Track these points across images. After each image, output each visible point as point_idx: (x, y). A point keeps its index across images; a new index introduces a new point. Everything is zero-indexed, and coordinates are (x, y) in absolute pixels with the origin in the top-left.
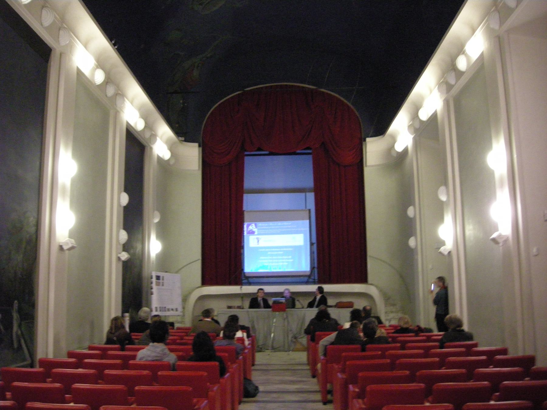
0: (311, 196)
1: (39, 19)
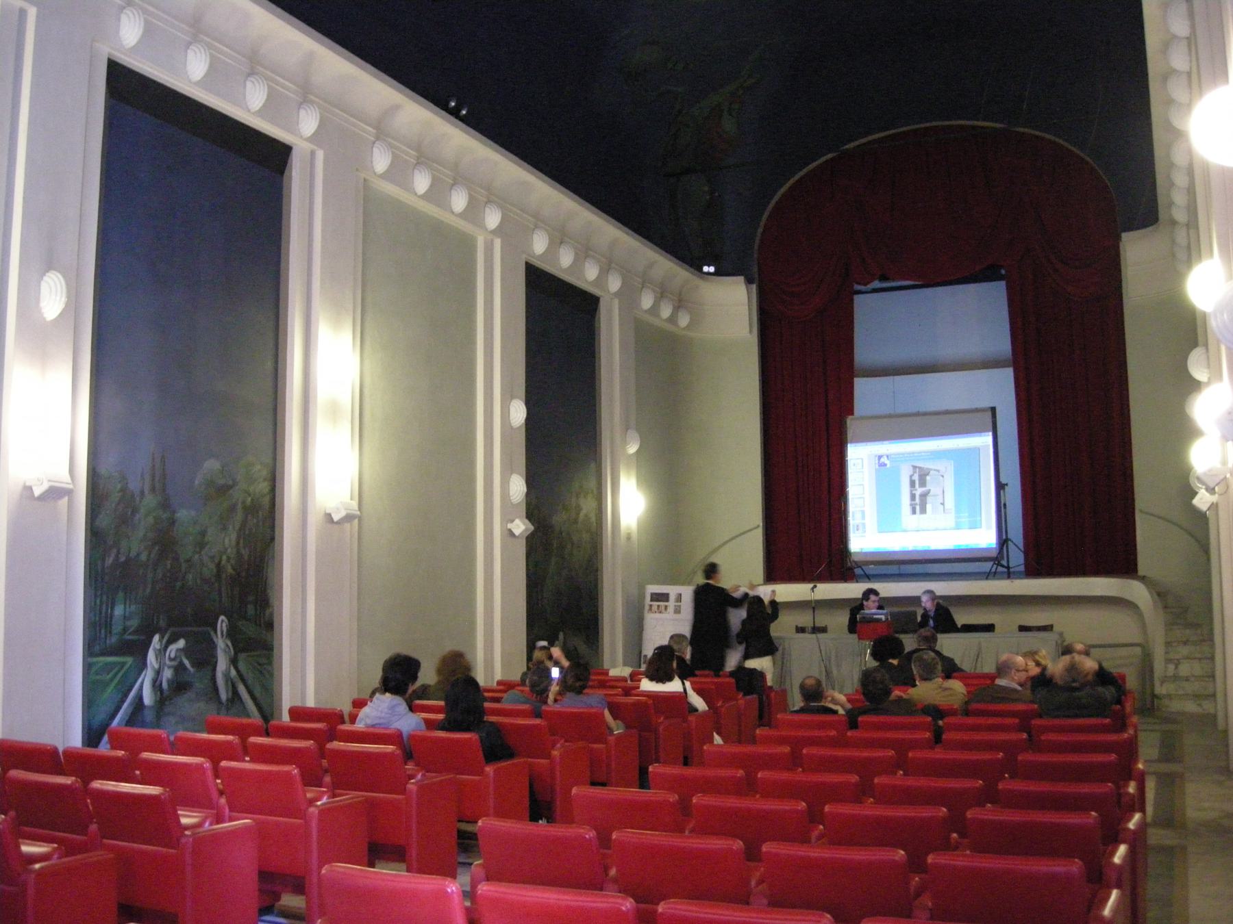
0: (1009, 372)
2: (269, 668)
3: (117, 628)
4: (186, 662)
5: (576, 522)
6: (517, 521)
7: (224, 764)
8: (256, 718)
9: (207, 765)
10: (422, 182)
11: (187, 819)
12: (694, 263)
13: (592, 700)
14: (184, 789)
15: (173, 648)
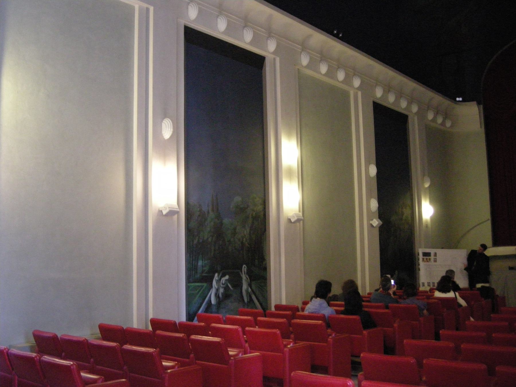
1: (242, 39)
3: (200, 270)
4: (230, 286)
5: (402, 219)
6: (375, 220)
7: (247, 328)
8: (260, 309)
9: (240, 329)
10: (324, 69)
11: (232, 352)
12: (453, 98)
13: (411, 302)
14: (230, 338)
15: (224, 280)
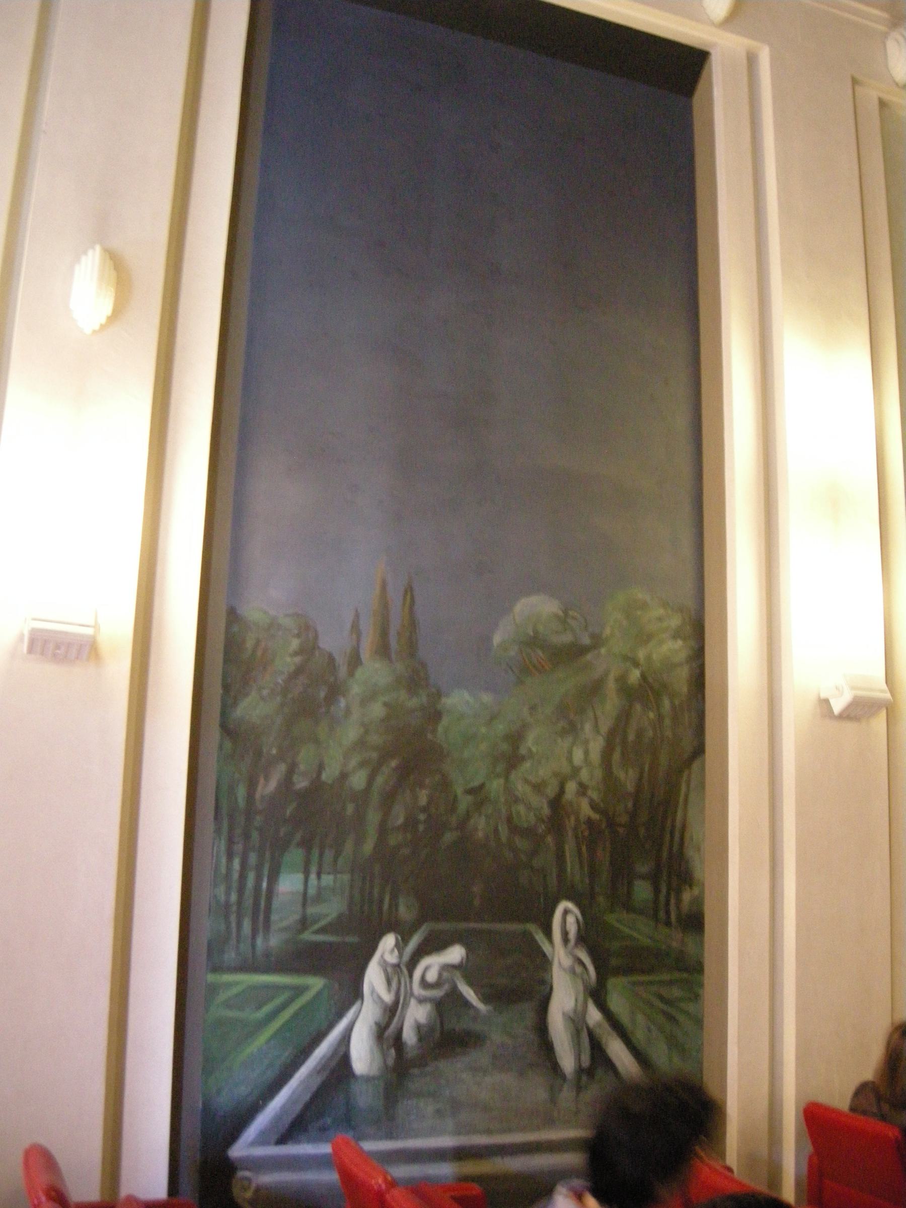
2: (691, 1007)
4: (469, 993)
15: (432, 966)
